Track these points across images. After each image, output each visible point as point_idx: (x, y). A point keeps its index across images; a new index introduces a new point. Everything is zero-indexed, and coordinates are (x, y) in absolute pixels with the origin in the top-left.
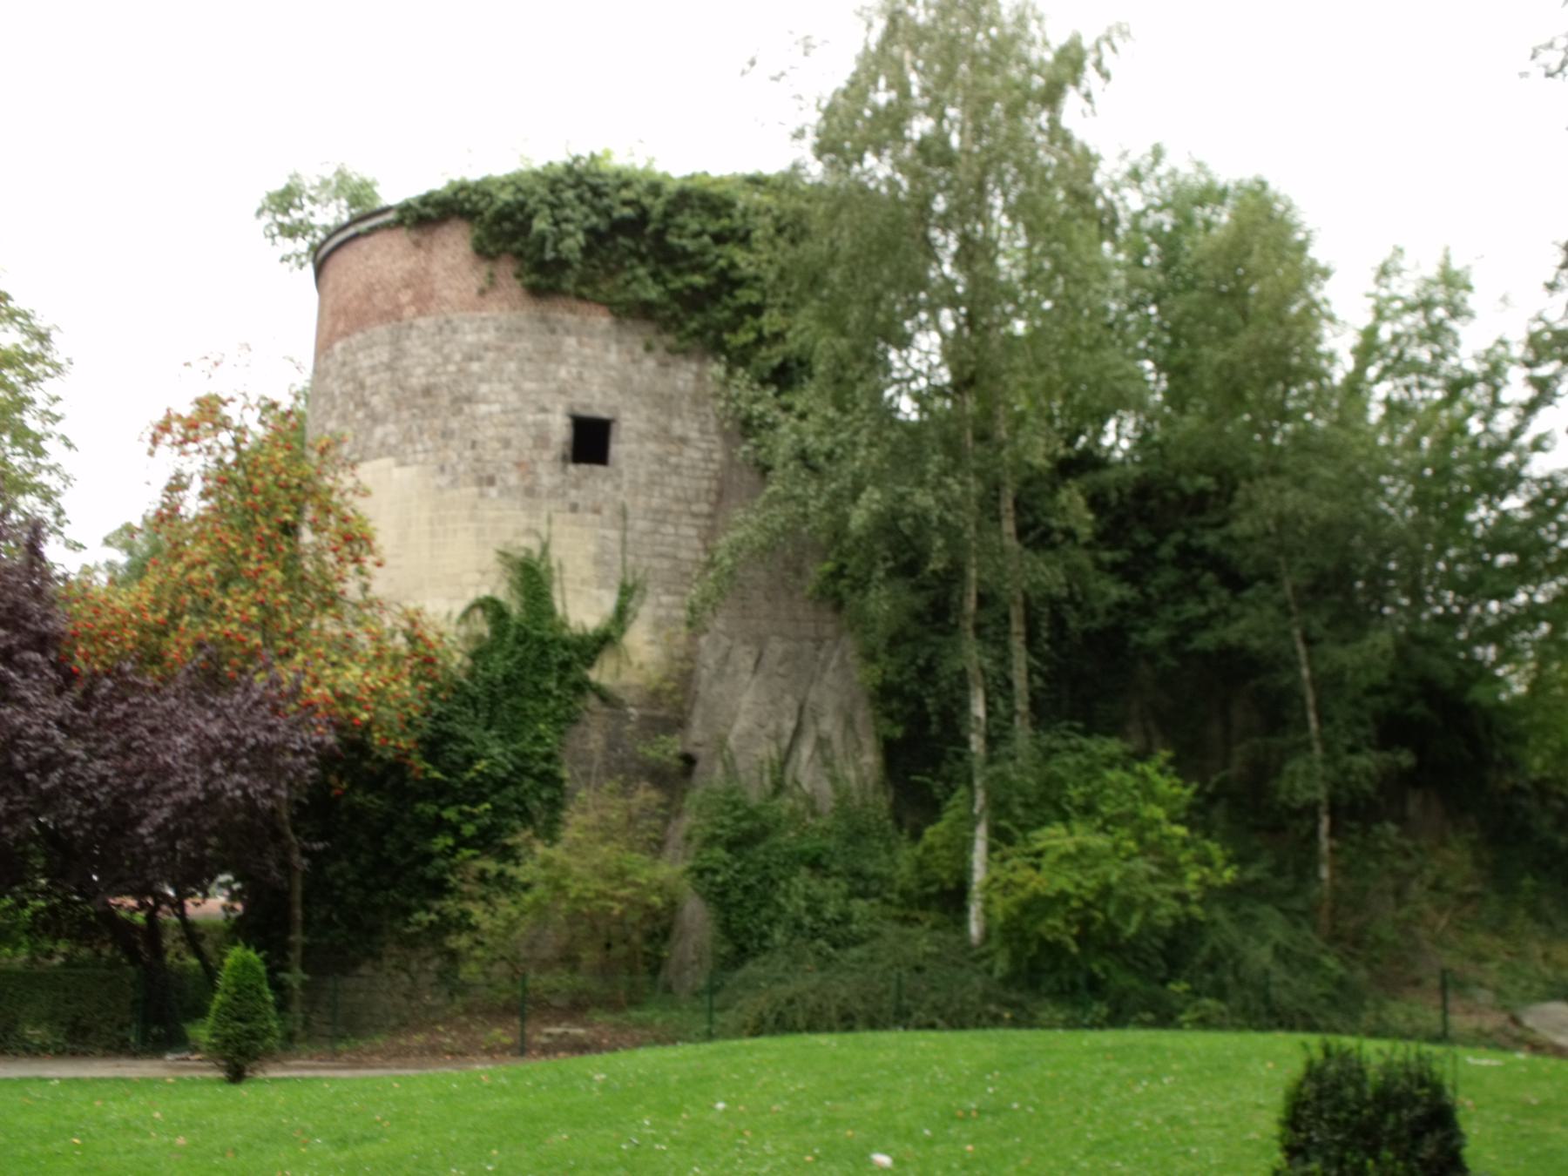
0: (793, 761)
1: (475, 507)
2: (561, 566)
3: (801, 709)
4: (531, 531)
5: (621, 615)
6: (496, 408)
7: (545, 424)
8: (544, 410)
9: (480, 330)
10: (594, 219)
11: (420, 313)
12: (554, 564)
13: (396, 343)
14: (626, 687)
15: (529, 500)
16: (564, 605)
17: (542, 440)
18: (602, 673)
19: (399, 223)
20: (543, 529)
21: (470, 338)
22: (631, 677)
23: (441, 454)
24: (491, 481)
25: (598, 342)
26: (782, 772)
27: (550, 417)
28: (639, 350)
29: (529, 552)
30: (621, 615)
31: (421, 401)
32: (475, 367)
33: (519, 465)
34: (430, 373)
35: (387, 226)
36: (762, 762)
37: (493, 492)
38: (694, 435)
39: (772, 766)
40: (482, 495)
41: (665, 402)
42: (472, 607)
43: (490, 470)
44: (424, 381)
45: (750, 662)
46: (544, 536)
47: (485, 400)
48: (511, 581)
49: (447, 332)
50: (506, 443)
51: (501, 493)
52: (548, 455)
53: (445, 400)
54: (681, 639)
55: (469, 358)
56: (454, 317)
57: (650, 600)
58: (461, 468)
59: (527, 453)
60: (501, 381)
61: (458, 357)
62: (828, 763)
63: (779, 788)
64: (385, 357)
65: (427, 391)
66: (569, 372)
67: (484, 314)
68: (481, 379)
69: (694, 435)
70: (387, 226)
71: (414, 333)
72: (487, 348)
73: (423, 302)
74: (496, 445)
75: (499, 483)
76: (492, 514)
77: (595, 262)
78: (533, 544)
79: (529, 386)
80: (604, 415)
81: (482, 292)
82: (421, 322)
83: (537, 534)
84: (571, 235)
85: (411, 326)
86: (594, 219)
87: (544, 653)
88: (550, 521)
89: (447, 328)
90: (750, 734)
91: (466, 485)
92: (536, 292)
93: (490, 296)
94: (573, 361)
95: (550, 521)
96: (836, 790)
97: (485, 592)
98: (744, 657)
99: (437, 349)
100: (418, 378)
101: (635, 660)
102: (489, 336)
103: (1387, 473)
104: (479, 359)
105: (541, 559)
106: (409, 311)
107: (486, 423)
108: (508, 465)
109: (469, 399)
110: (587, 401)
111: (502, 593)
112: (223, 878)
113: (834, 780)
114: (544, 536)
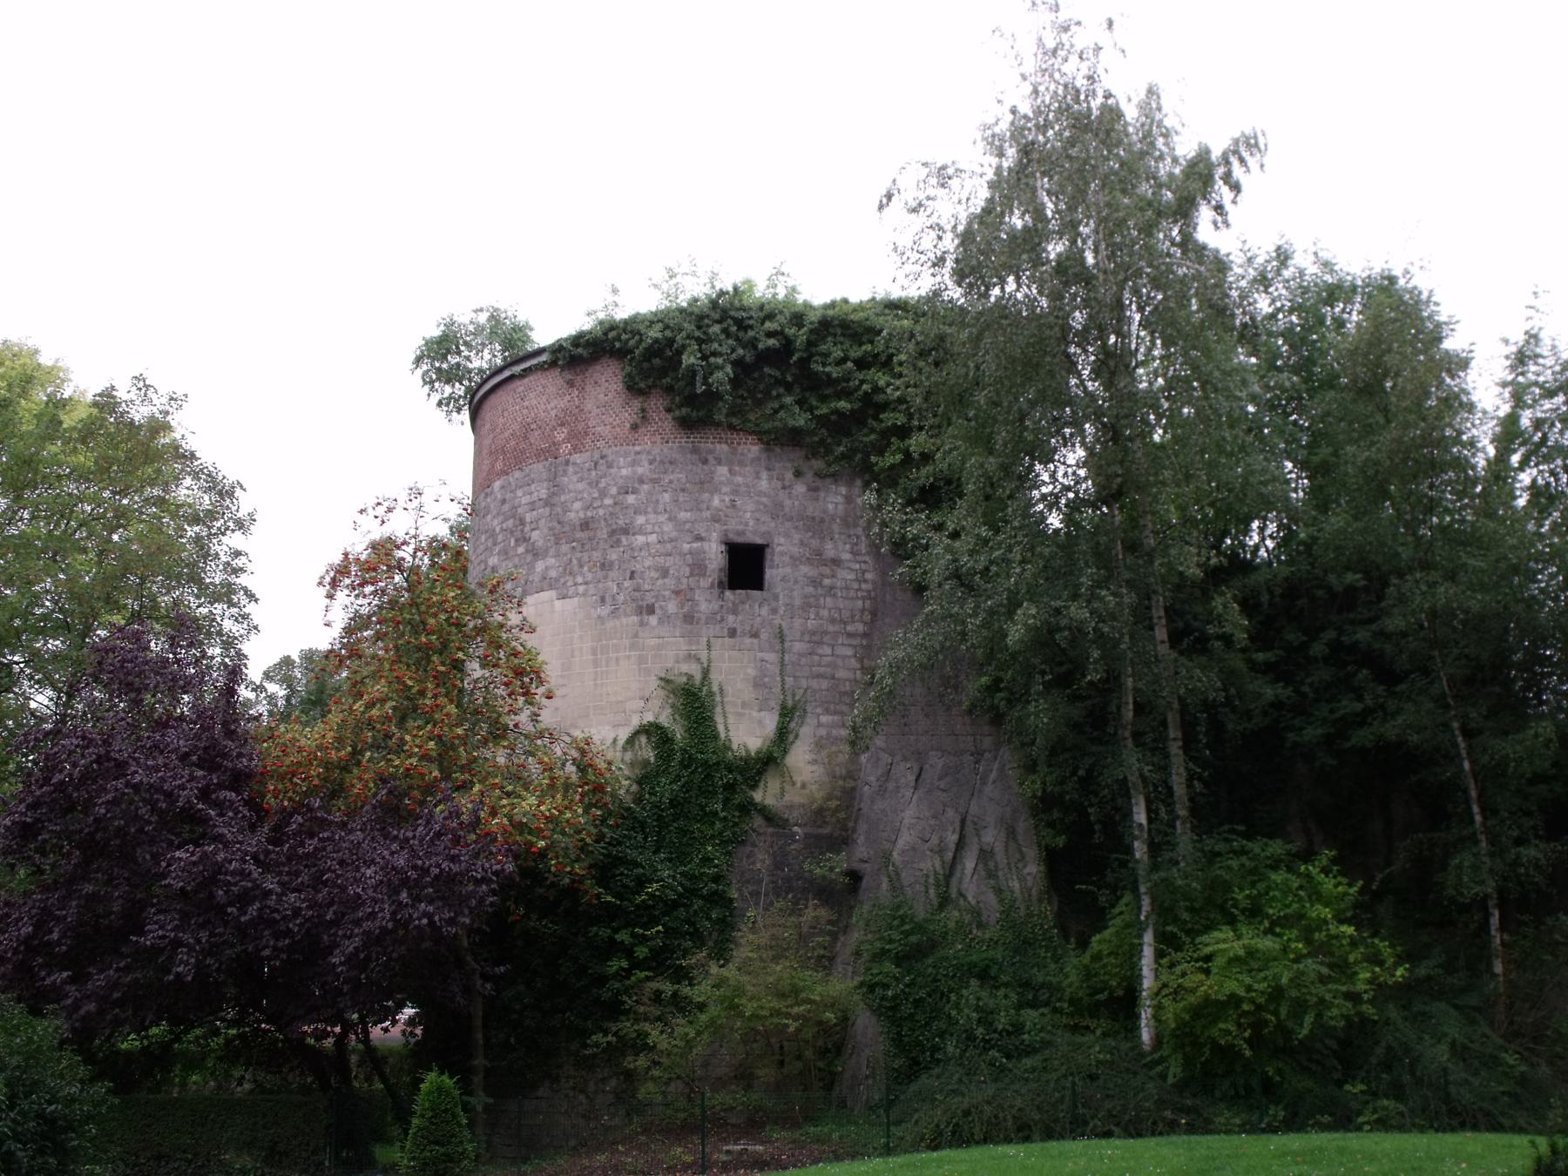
0: (958, 874)
1: (636, 636)
2: (721, 690)
6: (653, 538)
8: (699, 538)
9: (633, 464)
11: (575, 449)
12: (715, 688)
13: (553, 479)
14: (791, 807)
15: (689, 627)
17: (698, 568)
18: (767, 794)
19: (553, 364)
20: (704, 655)
21: (624, 472)
22: (794, 797)
24: (651, 610)
27: (706, 545)
28: (789, 475)
29: (690, 677)
30: (783, 737)
31: (579, 535)
32: (631, 499)
33: (677, 593)
35: (540, 368)
36: (927, 876)
37: (653, 620)
38: (846, 556)
41: (817, 526)
43: (649, 599)
44: (582, 515)
47: (641, 531)
49: (602, 467)
50: (665, 573)
52: (705, 583)
53: (603, 533)
57: (811, 720)
58: (621, 598)
59: (685, 581)
61: (614, 491)
62: (991, 875)
63: (945, 901)
64: (543, 493)
65: (585, 525)
67: (637, 448)
69: (846, 556)
70: (540, 368)
71: (571, 469)
73: (578, 438)
74: (654, 574)
75: (658, 611)
78: (695, 670)
79: (683, 515)
80: (759, 541)
81: (635, 427)
82: (577, 458)
85: (567, 463)
86: (741, 351)
87: (709, 776)
91: (626, 615)
92: (687, 425)
93: (642, 430)
94: (725, 489)
96: (1001, 901)
97: (649, 717)
100: (576, 513)
101: (798, 779)
106: (565, 448)
109: (626, 531)
110: (740, 527)
111: (665, 720)
113: (998, 891)
114: (704, 659)
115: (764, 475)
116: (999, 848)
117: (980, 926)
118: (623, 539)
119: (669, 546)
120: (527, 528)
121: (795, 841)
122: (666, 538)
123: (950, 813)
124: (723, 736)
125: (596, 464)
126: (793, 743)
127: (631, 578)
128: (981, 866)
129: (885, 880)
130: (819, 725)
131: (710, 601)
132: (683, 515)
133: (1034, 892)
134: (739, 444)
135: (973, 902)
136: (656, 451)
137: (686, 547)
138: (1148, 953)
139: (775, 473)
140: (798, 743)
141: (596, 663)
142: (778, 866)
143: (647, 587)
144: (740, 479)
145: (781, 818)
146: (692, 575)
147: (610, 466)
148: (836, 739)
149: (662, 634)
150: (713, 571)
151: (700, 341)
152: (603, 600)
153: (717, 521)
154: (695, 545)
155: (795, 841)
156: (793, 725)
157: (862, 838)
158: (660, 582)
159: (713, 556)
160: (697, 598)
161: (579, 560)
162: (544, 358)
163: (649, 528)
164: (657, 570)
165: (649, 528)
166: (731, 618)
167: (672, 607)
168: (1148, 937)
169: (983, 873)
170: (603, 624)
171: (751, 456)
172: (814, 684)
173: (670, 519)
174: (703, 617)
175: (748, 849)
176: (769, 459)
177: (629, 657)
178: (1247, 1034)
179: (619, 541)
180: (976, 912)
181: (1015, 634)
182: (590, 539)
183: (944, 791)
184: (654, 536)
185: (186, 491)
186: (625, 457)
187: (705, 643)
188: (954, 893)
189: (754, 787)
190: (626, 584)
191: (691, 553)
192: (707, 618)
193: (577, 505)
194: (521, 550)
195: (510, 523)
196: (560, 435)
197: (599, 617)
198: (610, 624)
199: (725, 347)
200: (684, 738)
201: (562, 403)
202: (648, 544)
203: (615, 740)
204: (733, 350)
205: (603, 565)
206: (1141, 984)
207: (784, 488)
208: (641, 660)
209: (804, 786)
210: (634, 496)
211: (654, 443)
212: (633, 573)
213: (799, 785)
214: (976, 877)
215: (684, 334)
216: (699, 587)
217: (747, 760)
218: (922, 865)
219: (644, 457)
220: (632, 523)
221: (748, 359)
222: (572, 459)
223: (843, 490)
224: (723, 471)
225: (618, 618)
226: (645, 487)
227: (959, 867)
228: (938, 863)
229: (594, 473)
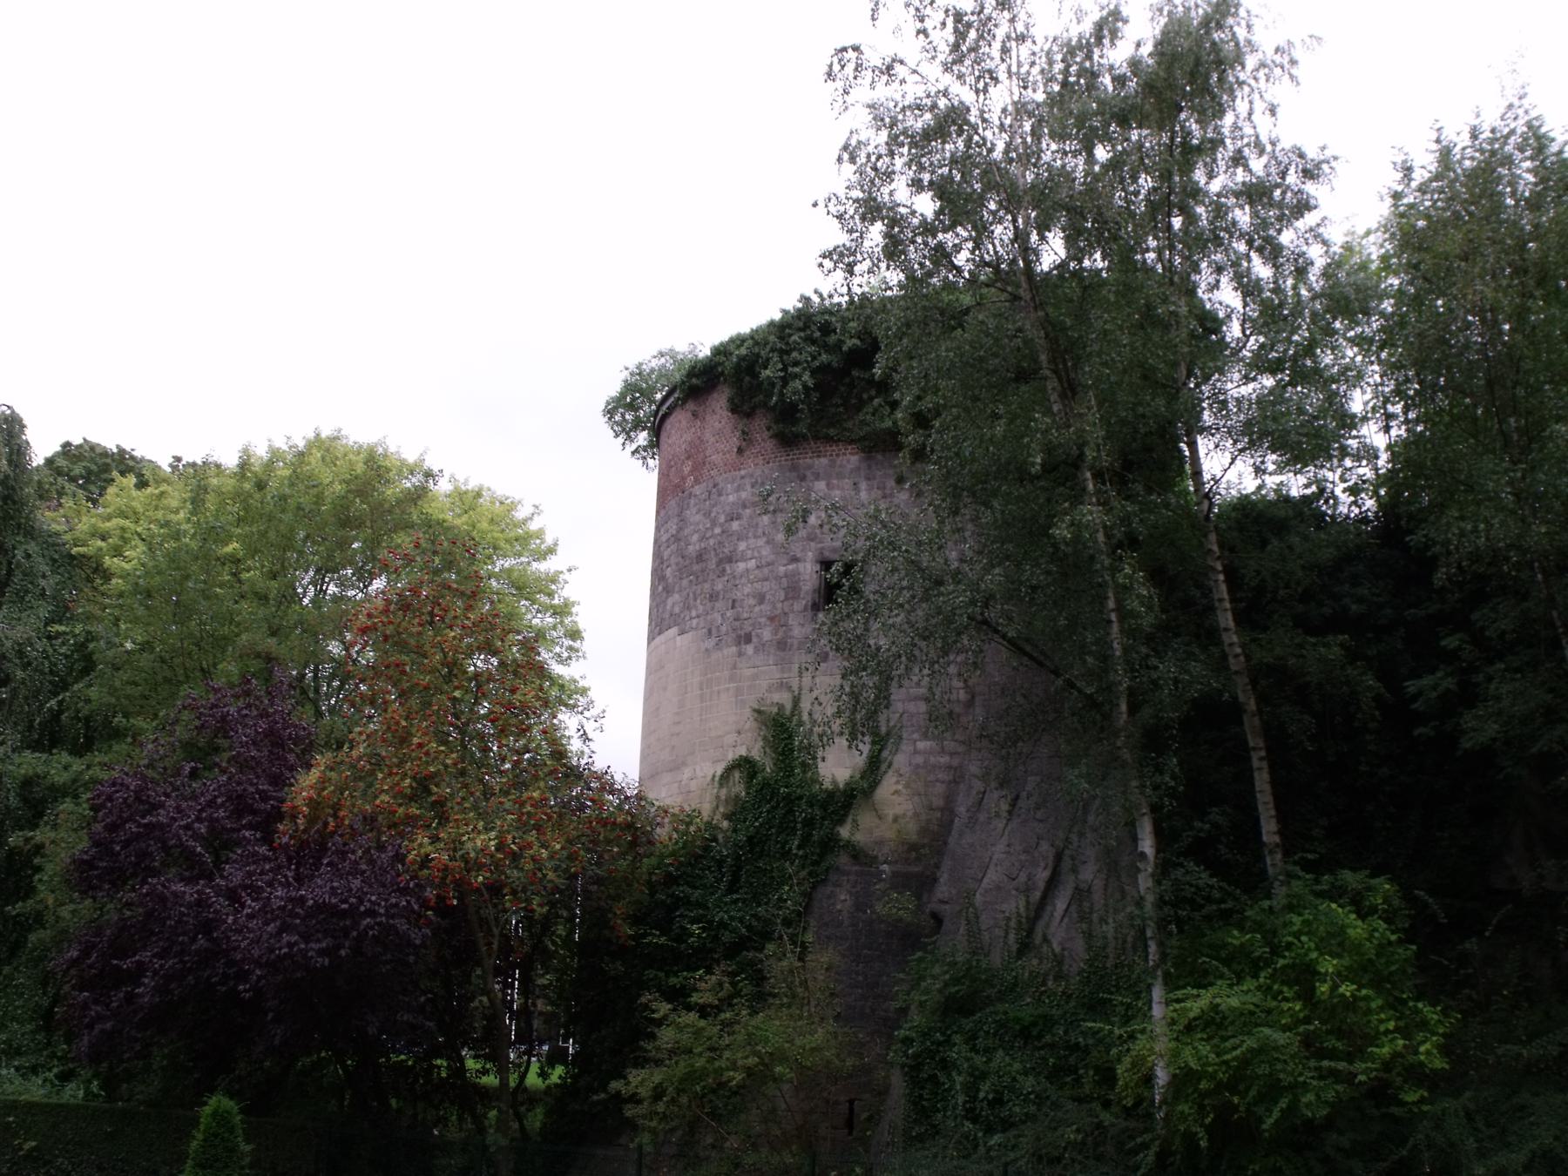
0: (1046, 917)
1: (735, 667)
3: (1058, 857)
4: (783, 686)
5: (874, 769)
6: (752, 564)
7: (796, 573)
8: (795, 560)
9: (739, 489)
10: (824, 357)
14: (880, 843)
15: (782, 654)
17: (792, 591)
18: (859, 830)
20: (795, 684)
21: (731, 498)
22: (887, 832)
23: (709, 617)
24: (748, 639)
25: (847, 483)
26: (1030, 932)
27: (801, 566)
28: (891, 483)
29: (781, 707)
30: (874, 769)
31: (696, 567)
32: (735, 525)
33: (772, 619)
34: (703, 538)
36: (1009, 919)
37: (749, 649)
39: (1020, 922)
40: (740, 654)
42: (729, 770)
43: (748, 628)
44: (697, 547)
45: (1005, 807)
46: (795, 688)
48: (765, 738)
50: (761, 599)
51: (756, 650)
52: (799, 606)
53: (712, 564)
54: (940, 789)
55: (731, 518)
56: (719, 479)
57: (906, 747)
58: (724, 629)
59: (779, 605)
60: (756, 537)
61: (722, 519)
62: (1084, 917)
63: (1025, 947)
65: (700, 557)
67: (743, 472)
68: (741, 537)
74: (752, 601)
75: (755, 640)
76: (748, 672)
78: (784, 698)
81: (740, 451)
84: (796, 376)
86: (824, 357)
87: (791, 811)
89: (716, 490)
90: (998, 888)
91: (728, 646)
92: (787, 441)
96: (1089, 948)
97: (743, 752)
98: (997, 802)
99: (707, 514)
100: (692, 549)
101: (890, 813)
103: (1022, 437)
104: (739, 518)
105: (793, 714)
107: (744, 580)
108: (763, 620)
109: (730, 560)
111: (756, 754)
113: (1089, 936)
114: (795, 688)
115: (863, 485)
116: (1098, 884)
117: (1058, 977)
119: (766, 570)
121: (881, 880)
122: (763, 562)
123: (1045, 846)
126: (885, 772)
128: (1073, 908)
129: (964, 922)
130: (916, 752)
131: (803, 625)
133: (1129, 939)
134: (838, 455)
135: (1057, 949)
136: (758, 472)
137: (782, 569)
139: (875, 483)
140: (890, 773)
141: (702, 698)
142: (859, 907)
143: (745, 615)
145: (866, 856)
146: (786, 599)
147: (720, 495)
148: (934, 766)
149: (759, 663)
150: (807, 593)
151: (782, 352)
152: (710, 631)
153: (812, 540)
154: (790, 567)
155: (881, 880)
156: (885, 754)
157: (946, 876)
158: (757, 609)
159: (807, 577)
160: (790, 622)
161: (694, 593)
164: (754, 597)
167: (767, 634)
169: (1075, 915)
170: (709, 656)
171: (850, 466)
172: (911, 707)
173: (768, 542)
174: (796, 642)
175: (829, 889)
176: (869, 467)
177: (728, 689)
178: (1208, 1120)
179: (724, 570)
180: (1059, 960)
181: (230, 649)
182: (703, 571)
183: (1041, 821)
186: (733, 482)
187: (796, 670)
188: (1038, 939)
189: (841, 822)
190: (729, 614)
191: (786, 576)
192: (800, 643)
197: (707, 650)
198: (716, 655)
199: (804, 354)
200: (773, 771)
201: (688, 437)
203: (714, 776)
204: (814, 358)
205: (711, 596)
207: (884, 497)
208: (738, 692)
209: (896, 819)
211: (756, 465)
213: (890, 818)
214: (1066, 920)
215: (768, 348)
216: (793, 611)
217: (831, 794)
218: (1005, 907)
219: (747, 481)
220: (735, 550)
221: (835, 364)
225: (720, 649)
226: (748, 511)
227: (1049, 908)
228: (1022, 904)
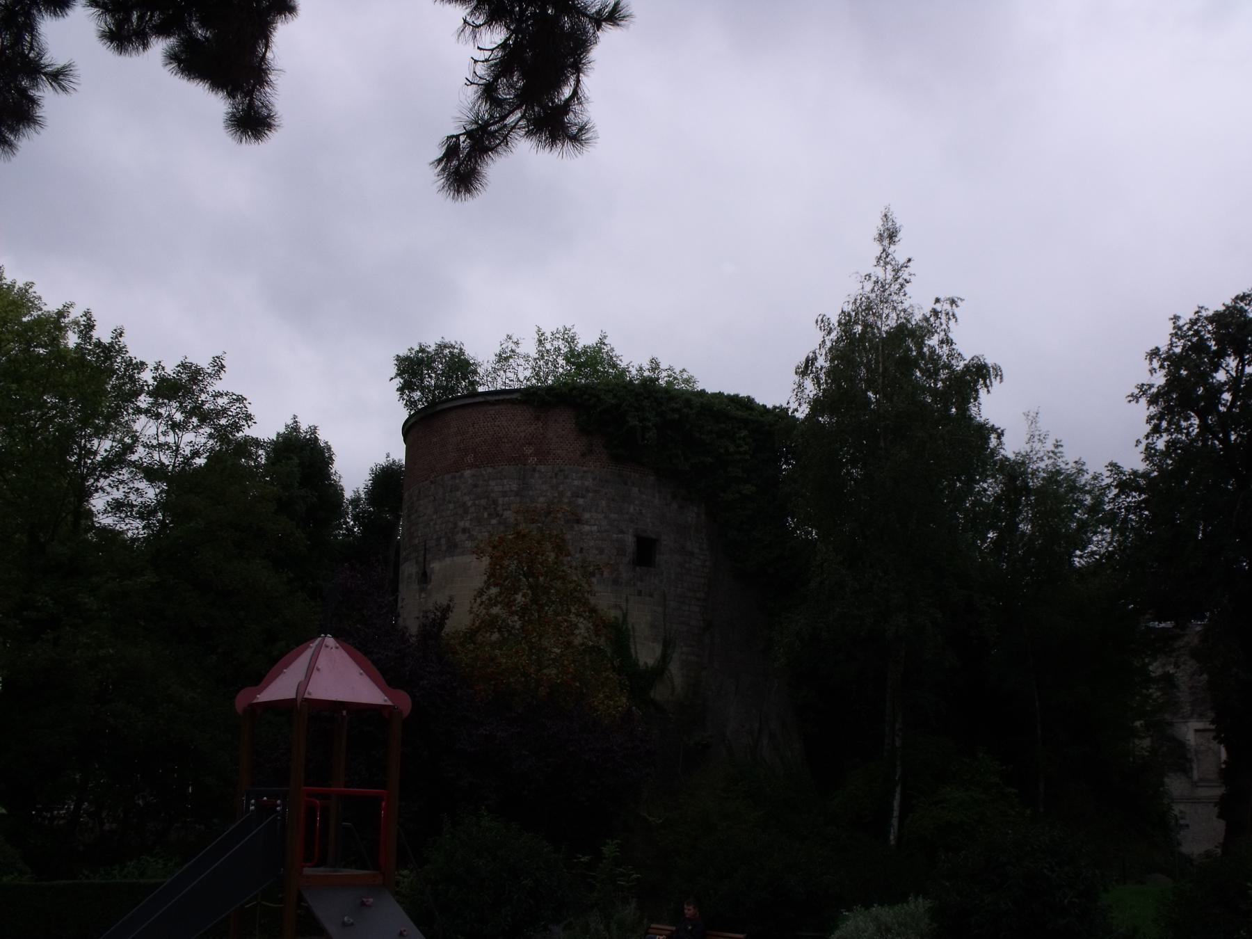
2: (633, 628)
4: (616, 606)
8: (622, 532)
12: (630, 627)
16: (636, 653)
21: (576, 483)
30: (665, 659)
32: (581, 501)
35: (512, 402)
38: (697, 551)
47: (587, 523)
50: (601, 551)
61: (569, 494)
64: (515, 487)
66: (635, 509)
67: (585, 469)
69: (697, 551)
70: (512, 402)
71: (537, 475)
72: (588, 491)
77: (1183, 667)
79: (613, 516)
80: (654, 536)
81: (583, 455)
82: (541, 468)
83: (621, 609)
85: (534, 470)
88: (627, 600)
94: (637, 502)
95: (627, 600)
102: (589, 483)
104: (583, 497)
106: (532, 460)
112: (136, 798)
118: (575, 526)
120: (499, 508)
124: (634, 656)
125: (556, 474)
126: (669, 662)
127: (582, 549)
132: (613, 516)
138: (898, 796)
144: (644, 496)
147: (566, 477)
154: (620, 536)
162: (514, 396)
163: (593, 521)
165: (593, 521)
166: (639, 583)
168: (898, 789)
184: (596, 527)
185: (1188, 748)
193: (542, 499)
194: (494, 521)
195: (483, 502)
196: (529, 450)
202: (591, 532)
206: (893, 814)
210: (583, 500)
212: (582, 549)
222: (538, 467)
223: (696, 509)
224: (635, 490)
226: (590, 494)
229: (555, 480)
